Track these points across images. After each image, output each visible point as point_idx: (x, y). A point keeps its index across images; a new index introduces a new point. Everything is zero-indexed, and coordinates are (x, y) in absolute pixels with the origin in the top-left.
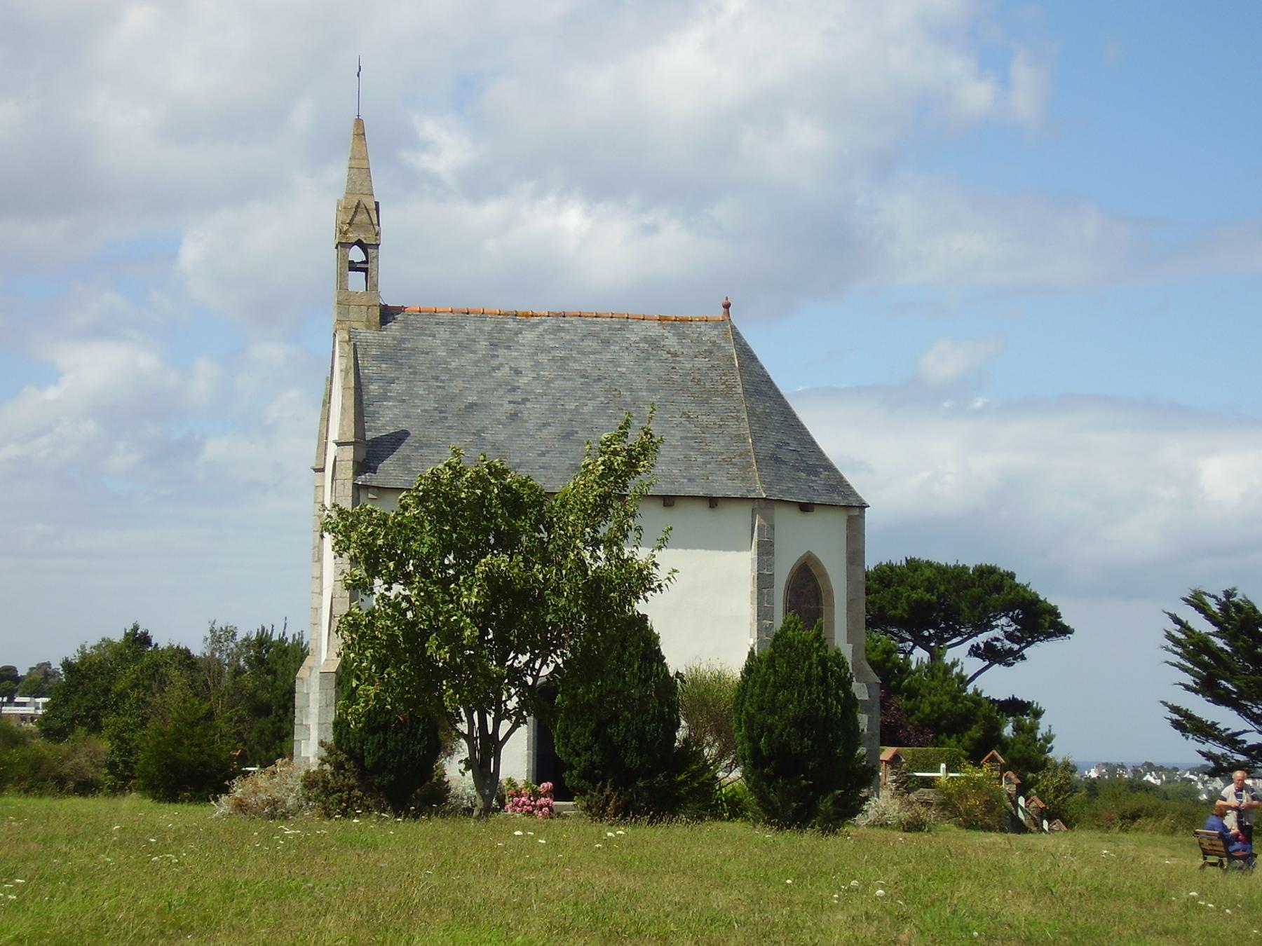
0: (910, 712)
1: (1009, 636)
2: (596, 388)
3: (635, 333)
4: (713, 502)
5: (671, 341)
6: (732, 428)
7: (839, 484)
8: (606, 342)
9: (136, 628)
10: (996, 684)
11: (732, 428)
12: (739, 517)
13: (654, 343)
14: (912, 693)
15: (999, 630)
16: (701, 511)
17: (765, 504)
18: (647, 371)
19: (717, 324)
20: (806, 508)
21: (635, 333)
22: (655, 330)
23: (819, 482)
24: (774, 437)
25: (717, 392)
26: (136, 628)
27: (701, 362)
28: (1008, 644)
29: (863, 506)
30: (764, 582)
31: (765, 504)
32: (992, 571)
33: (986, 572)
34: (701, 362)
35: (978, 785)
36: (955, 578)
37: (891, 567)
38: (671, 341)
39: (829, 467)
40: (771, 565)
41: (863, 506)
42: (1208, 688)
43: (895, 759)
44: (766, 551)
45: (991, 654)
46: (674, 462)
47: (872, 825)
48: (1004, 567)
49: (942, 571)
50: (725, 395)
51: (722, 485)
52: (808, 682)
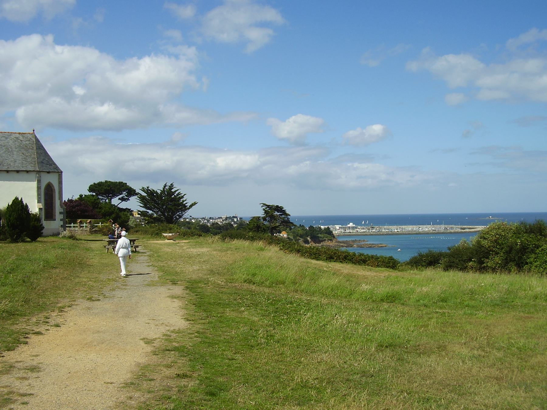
0: (100, 212)
1: (126, 196)
2: (3, 148)
3: (13, 136)
4: (18, 172)
5: (21, 138)
6: (33, 156)
7: (57, 168)
8: (7, 138)
9: (171, 187)
10: (123, 205)
11: (33, 156)
12: (33, 175)
13: (17, 138)
14: (100, 208)
15: (124, 194)
16: (25, 174)
17: (39, 172)
18: (15, 144)
19: (31, 134)
20: (49, 172)
21: (13, 136)
22: (18, 135)
23: (52, 167)
24: (42, 158)
25: (30, 149)
26: (171, 187)
27: (27, 142)
28: (126, 197)
29: (62, 172)
30: (39, 188)
31: (39, 172)
32: (122, 182)
33: (121, 183)
34: (27, 142)
35: (106, 227)
36: (115, 184)
37: (102, 182)
38: (21, 138)
39: (55, 164)
40: (40, 185)
41: (62, 172)
42: (145, 207)
43: (90, 221)
44: (39, 182)
45: (123, 199)
46: (19, 163)
47: (62, 237)
48: (92, 183)
49: (112, 183)
50: (32, 149)
51: (30, 168)
52: (18, 210)
